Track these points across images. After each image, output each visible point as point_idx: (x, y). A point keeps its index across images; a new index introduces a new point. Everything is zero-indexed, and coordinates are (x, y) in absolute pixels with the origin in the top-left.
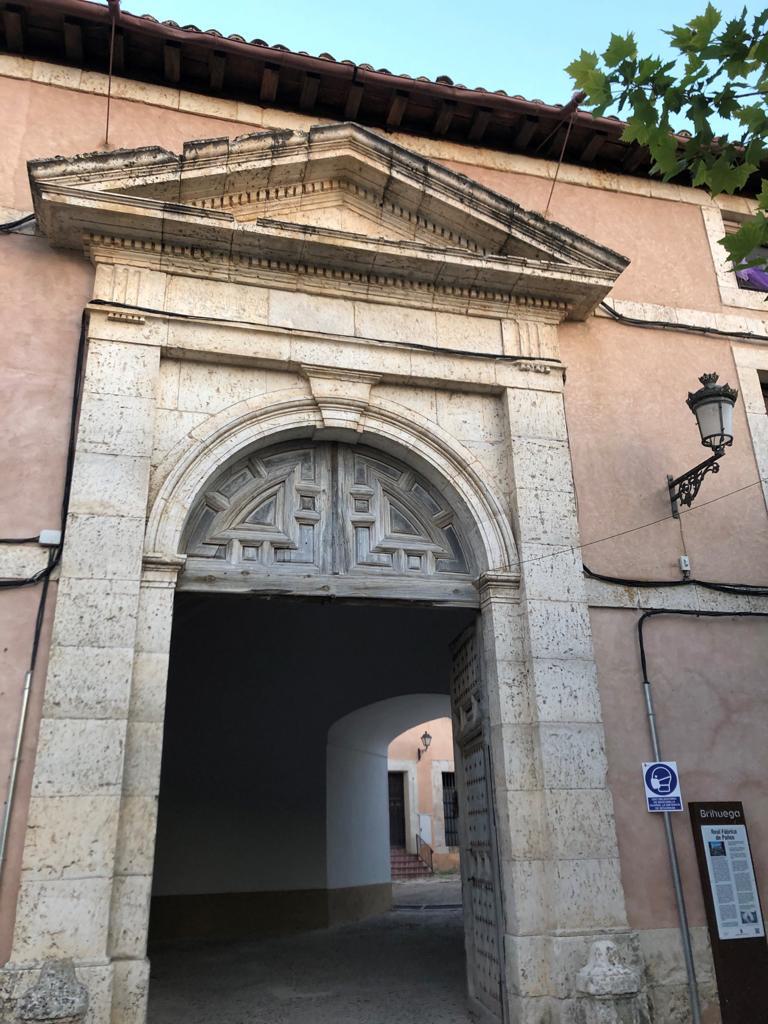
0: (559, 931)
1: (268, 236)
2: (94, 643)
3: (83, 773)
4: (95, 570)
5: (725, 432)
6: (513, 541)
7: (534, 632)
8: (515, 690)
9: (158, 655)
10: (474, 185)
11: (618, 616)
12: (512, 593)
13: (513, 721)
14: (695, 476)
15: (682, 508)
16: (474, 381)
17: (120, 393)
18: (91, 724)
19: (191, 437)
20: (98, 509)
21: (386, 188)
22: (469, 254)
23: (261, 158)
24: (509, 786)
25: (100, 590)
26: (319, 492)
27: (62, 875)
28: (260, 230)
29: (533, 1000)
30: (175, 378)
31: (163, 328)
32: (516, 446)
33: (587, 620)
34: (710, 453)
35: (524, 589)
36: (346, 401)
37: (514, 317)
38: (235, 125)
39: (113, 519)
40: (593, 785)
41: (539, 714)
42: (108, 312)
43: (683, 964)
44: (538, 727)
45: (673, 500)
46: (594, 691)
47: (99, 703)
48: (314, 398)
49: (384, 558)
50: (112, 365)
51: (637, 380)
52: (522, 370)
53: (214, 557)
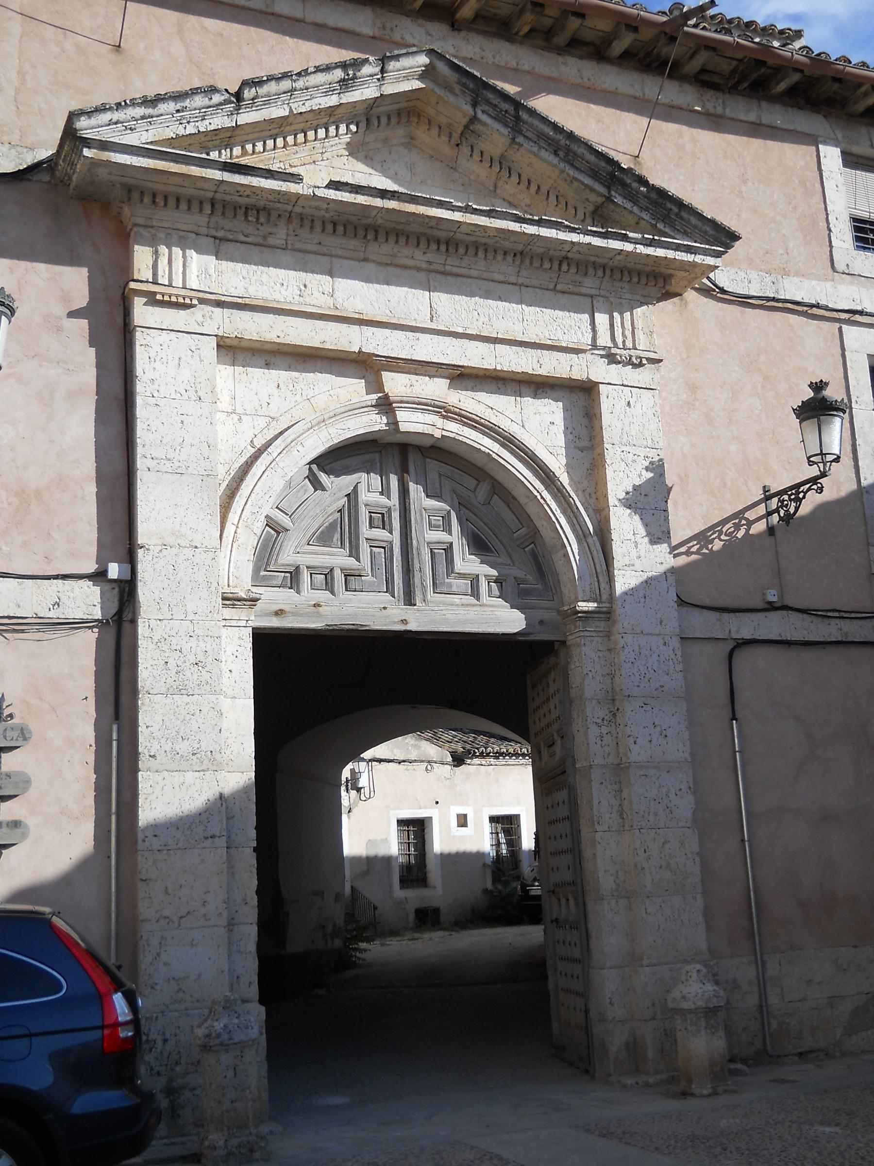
2: (181, 690)
3: (187, 826)
8: (604, 730)
12: (602, 625)
13: (602, 762)
18: (190, 776)
20: (170, 540)
21: (466, 127)
23: (326, 93)
27: (179, 925)
28: (332, 194)
33: (679, 654)
34: (814, 471)
35: (615, 622)
37: (608, 295)
39: (186, 551)
40: (680, 825)
47: (194, 754)
50: (165, 360)
51: (737, 368)
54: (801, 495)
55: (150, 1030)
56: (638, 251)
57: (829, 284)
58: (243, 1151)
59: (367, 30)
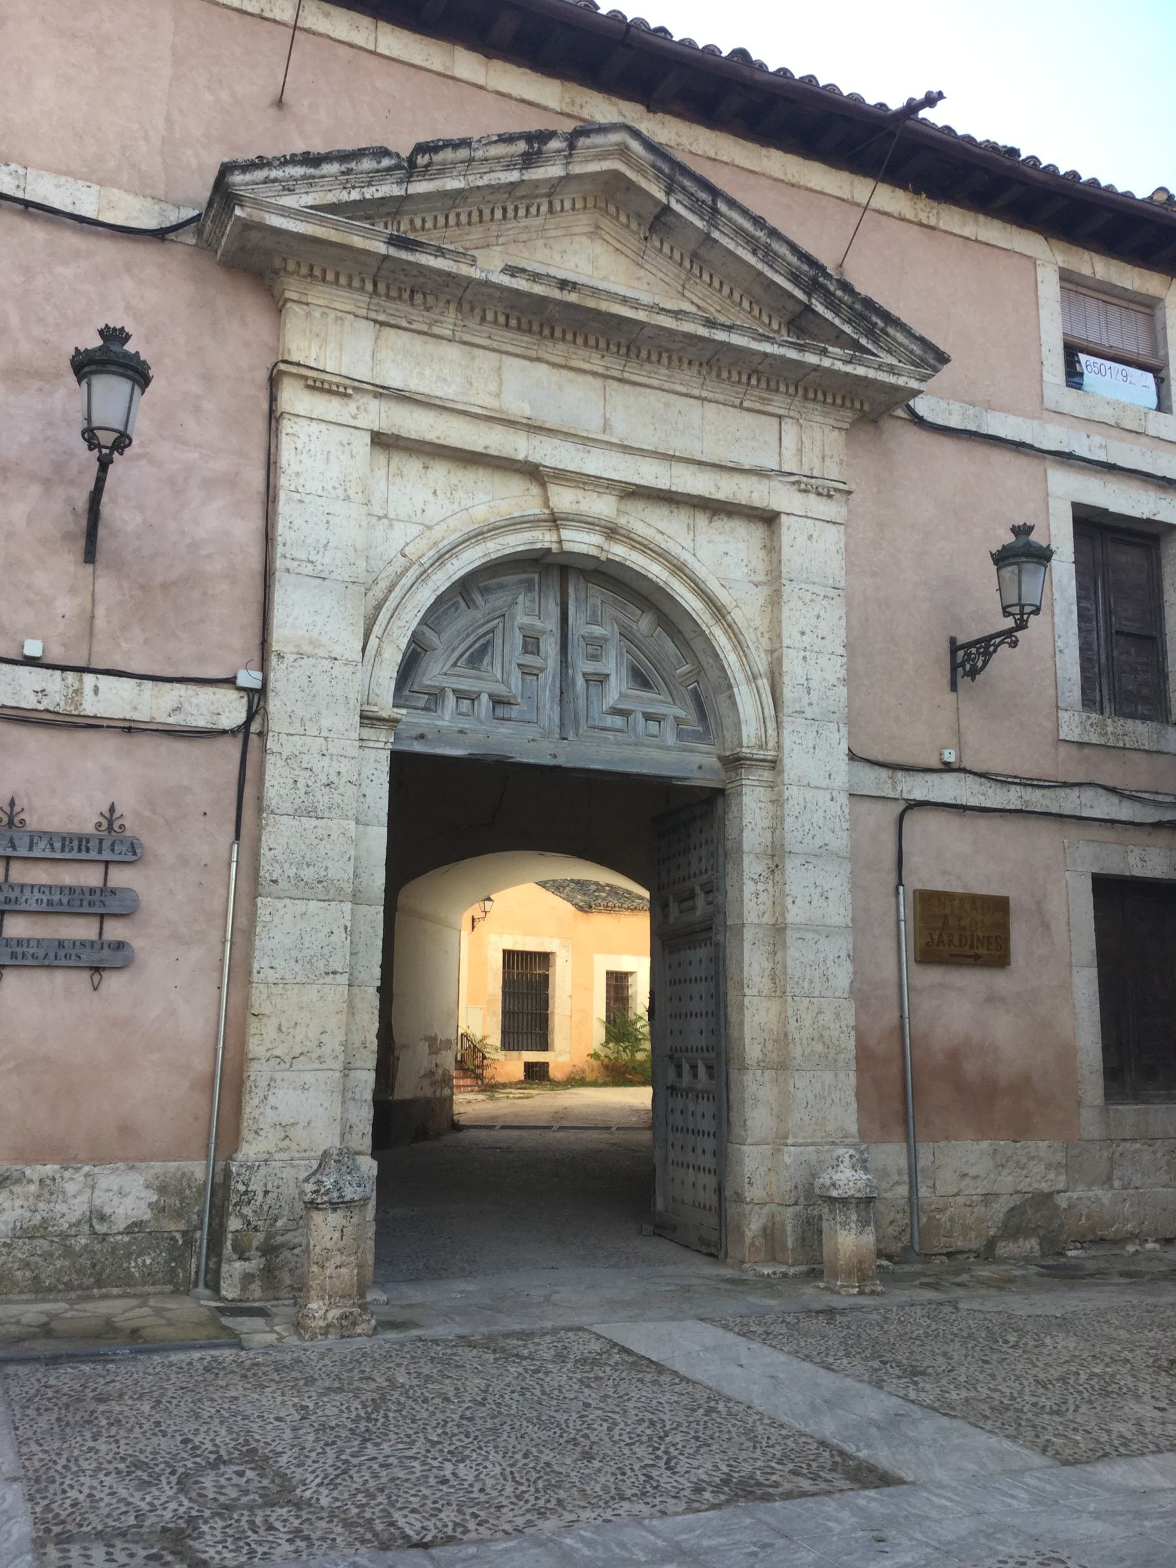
0: (790, 1141)
1: (517, 290)
2: (311, 812)
3: (307, 959)
4: (308, 725)
6: (773, 713)
7: (789, 823)
8: (761, 887)
9: (375, 828)
10: (773, 233)
11: (878, 807)
12: (767, 775)
13: (756, 921)
14: (986, 646)
16: (744, 503)
17: (324, 494)
18: (313, 905)
19: (404, 556)
20: (307, 648)
22: (760, 335)
23: (508, 168)
24: (747, 991)
25: (314, 750)
26: (545, 633)
28: (506, 280)
29: (757, 1207)
30: (384, 471)
31: (374, 404)
32: (787, 590)
33: (847, 811)
34: (1009, 623)
35: (781, 772)
36: (590, 520)
37: (798, 416)
38: (451, 82)
39: (325, 662)
40: (837, 994)
41: (787, 915)
42: (306, 378)
43: (906, 1178)
44: (784, 929)
46: (847, 892)
47: (320, 882)
48: (553, 513)
49: (619, 721)
52: (800, 491)
53: (422, 709)
54: (991, 649)
55: (250, 1179)
56: (836, 368)
57: (1036, 423)
58: (344, 1323)
59: (554, 104)
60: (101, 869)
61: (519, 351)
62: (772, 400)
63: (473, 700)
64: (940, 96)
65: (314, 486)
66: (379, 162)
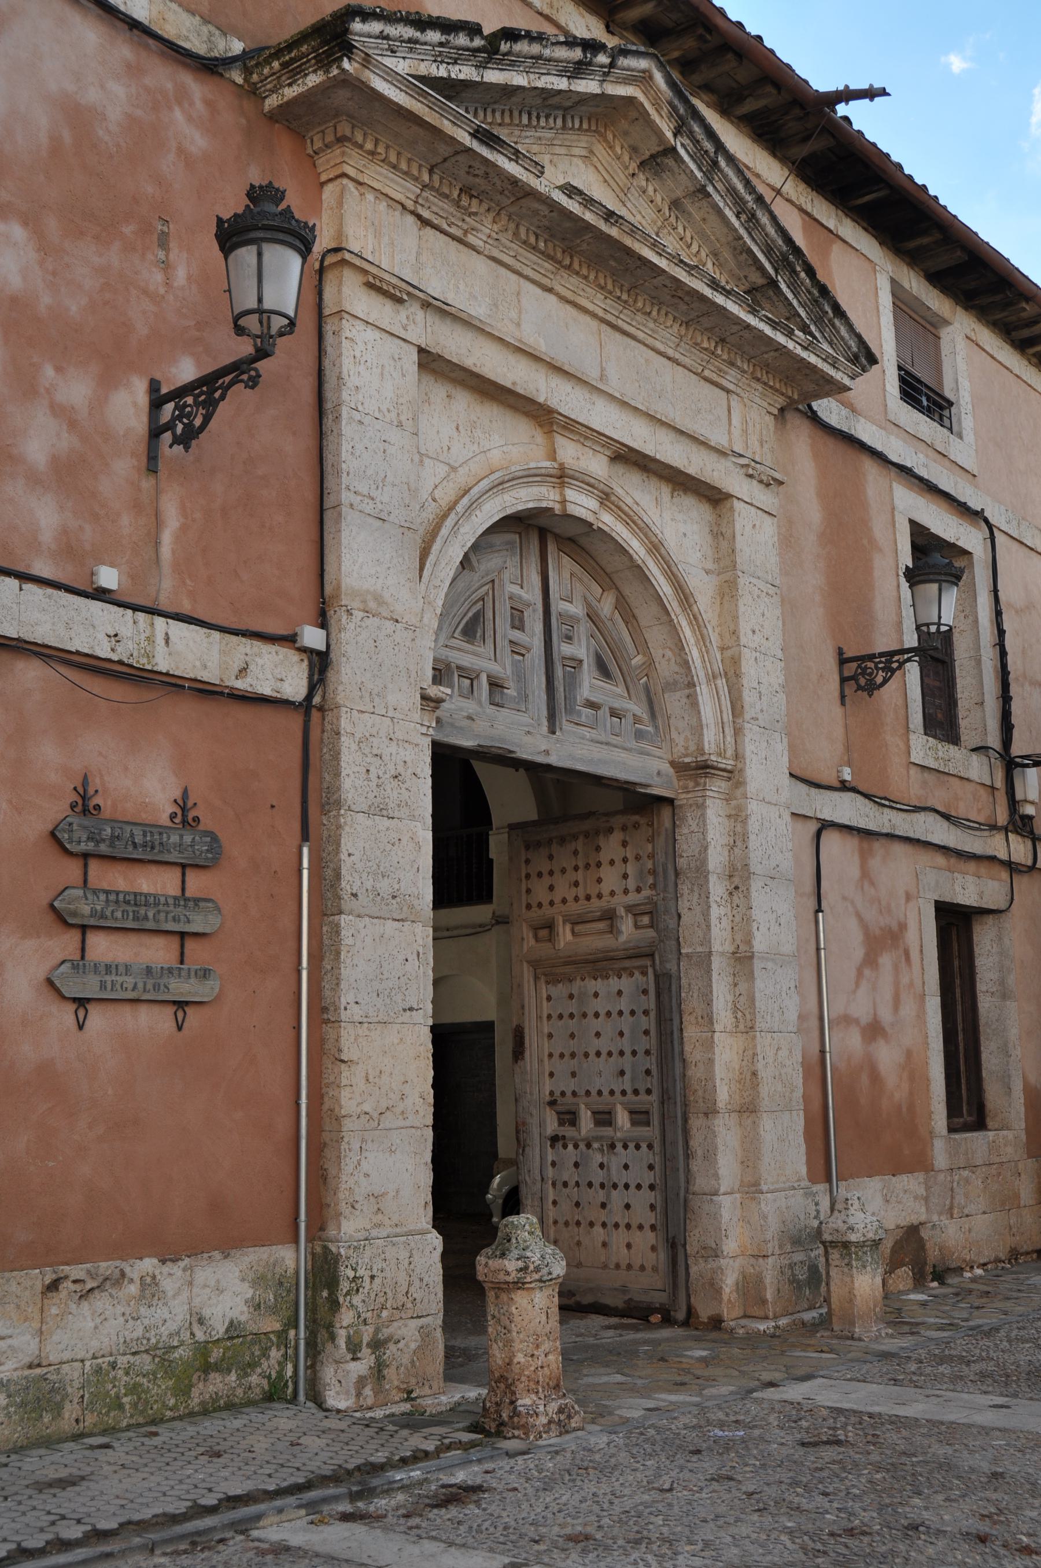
5: (942, 621)
13: (721, 949)
15: (169, 450)
19: (434, 500)
21: (653, 157)
34: (245, 348)
36: (592, 481)
42: (365, 272)
44: (752, 957)
45: (155, 433)
47: (394, 897)
60: (177, 872)
61: (537, 277)
62: (726, 373)
63: (472, 680)
64: (883, 92)
65: (371, 406)
66: (472, 40)
